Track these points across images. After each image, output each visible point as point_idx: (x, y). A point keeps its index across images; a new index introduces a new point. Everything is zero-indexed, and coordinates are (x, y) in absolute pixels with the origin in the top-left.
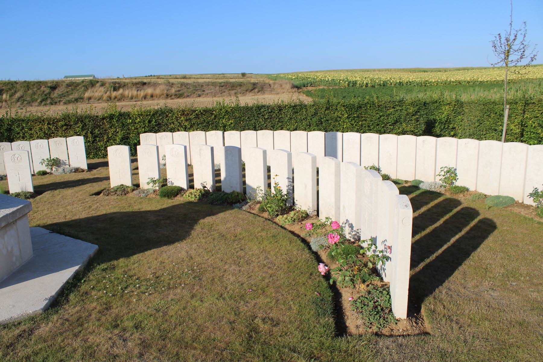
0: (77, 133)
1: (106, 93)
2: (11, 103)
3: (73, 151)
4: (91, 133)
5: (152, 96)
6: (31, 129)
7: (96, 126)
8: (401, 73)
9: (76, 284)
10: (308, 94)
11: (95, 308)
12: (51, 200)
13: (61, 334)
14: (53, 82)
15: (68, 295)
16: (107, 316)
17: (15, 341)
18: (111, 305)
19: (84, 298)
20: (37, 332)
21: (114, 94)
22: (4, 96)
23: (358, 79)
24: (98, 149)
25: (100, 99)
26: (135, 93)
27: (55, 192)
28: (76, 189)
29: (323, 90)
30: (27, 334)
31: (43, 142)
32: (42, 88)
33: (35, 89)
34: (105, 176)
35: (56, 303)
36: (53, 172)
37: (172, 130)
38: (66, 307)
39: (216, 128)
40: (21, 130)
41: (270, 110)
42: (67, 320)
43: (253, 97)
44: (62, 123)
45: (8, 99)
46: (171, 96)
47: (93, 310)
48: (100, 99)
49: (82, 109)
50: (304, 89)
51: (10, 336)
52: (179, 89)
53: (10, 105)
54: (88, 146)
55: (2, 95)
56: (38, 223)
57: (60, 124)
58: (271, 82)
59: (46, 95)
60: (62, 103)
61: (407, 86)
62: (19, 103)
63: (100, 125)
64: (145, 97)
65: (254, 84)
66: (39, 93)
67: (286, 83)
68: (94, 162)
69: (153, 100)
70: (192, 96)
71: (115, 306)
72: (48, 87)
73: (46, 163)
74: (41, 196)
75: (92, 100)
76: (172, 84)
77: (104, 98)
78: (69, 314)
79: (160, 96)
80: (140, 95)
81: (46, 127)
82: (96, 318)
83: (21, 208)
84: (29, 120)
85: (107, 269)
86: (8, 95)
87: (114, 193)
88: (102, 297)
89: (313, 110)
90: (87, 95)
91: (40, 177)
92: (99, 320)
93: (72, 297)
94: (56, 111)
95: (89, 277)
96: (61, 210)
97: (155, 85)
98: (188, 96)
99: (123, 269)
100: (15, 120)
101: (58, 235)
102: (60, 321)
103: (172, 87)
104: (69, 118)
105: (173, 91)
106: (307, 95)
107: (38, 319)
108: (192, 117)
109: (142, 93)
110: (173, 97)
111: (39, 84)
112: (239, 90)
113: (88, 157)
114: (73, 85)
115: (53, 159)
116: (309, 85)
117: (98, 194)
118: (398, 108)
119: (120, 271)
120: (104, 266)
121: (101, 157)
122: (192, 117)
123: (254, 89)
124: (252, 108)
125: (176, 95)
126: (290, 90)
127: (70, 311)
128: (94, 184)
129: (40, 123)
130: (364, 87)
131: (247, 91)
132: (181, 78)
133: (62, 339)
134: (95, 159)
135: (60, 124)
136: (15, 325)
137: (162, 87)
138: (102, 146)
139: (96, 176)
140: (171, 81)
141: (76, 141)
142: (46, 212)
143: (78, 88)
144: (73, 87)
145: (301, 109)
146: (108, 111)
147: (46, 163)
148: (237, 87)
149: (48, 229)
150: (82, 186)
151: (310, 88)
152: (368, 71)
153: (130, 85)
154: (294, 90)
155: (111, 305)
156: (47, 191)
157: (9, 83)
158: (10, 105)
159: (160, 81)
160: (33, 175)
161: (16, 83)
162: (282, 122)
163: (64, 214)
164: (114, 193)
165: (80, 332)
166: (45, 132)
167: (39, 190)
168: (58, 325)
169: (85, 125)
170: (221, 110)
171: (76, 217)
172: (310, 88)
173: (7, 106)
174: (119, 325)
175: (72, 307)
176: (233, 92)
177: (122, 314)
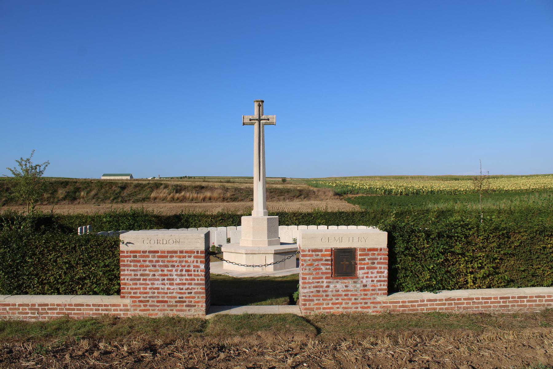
1: (170, 194)
2: (88, 200)
5: (210, 199)
6: (200, 221)
8: (433, 182)
10: (349, 201)
21: (177, 195)
22: (82, 194)
23: (394, 187)
33: (107, 189)
37: (288, 225)
44: (220, 218)
46: (227, 199)
48: (164, 199)
50: (345, 195)
60: (131, 202)
61: (434, 195)
62: (94, 200)
64: (204, 200)
65: (300, 191)
67: (329, 191)
69: (211, 202)
70: (246, 200)
72: (119, 187)
75: (157, 200)
76: (227, 189)
77: (168, 199)
79: (217, 199)
81: (209, 220)
89: (373, 215)
90: (153, 195)
97: (212, 189)
98: (242, 200)
105: (228, 194)
106: (348, 202)
108: (300, 217)
109: (201, 196)
112: (287, 196)
116: (349, 193)
118: (426, 214)
122: (300, 217)
123: (300, 195)
124: (336, 213)
125: (231, 199)
126: (333, 197)
130: (399, 195)
137: (220, 191)
140: (227, 185)
145: (366, 214)
151: (350, 196)
153: (190, 188)
157: (85, 182)
159: (217, 185)
169: (234, 220)
172: (350, 196)
176: (282, 197)
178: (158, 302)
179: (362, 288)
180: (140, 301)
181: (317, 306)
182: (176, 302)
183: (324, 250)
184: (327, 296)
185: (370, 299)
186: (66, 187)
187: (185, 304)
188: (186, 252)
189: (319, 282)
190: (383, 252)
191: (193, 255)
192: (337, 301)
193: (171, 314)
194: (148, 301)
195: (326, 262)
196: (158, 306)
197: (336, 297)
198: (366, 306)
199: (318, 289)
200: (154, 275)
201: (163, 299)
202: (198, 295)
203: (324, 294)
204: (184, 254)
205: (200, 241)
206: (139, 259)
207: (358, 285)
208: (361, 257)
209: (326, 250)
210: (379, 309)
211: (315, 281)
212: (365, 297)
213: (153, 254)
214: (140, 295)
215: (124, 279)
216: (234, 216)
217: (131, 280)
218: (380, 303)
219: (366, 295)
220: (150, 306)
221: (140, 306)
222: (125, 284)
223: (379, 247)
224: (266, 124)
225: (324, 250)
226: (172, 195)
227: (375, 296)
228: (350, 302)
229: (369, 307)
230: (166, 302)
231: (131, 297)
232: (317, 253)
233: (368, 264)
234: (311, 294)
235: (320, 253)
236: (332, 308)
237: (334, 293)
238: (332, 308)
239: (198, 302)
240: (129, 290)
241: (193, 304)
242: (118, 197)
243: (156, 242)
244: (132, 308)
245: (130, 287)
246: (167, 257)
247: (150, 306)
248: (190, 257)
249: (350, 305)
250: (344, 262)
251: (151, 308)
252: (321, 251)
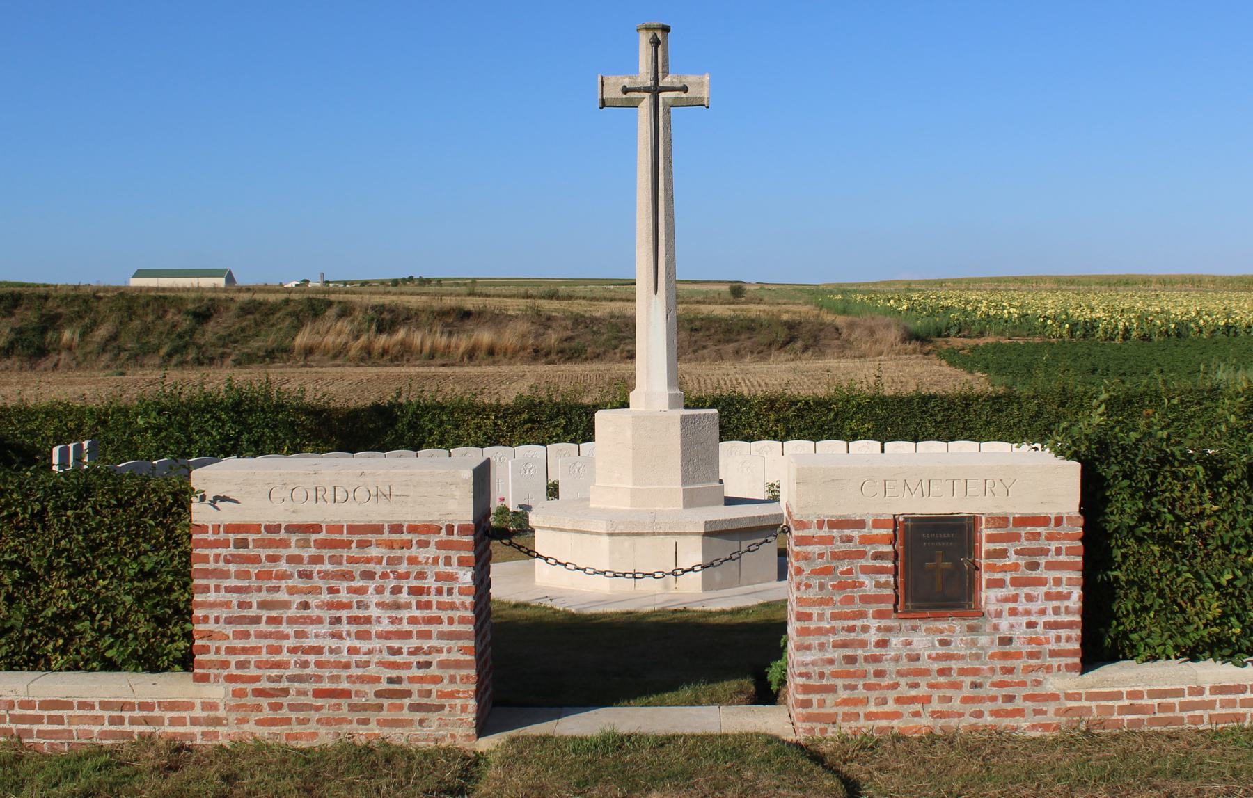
1: (357, 337)
2: (85, 355)
5: (491, 352)
6: (457, 427)
10: (954, 358)
14: (201, 300)
21: (382, 340)
22: (67, 335)
23: (1101, 315)
26: (442, 341)
29: (997, 348)
32: (169, 316)
33: (150, 318)
37: (749, 439)
39: (838, 437)
41: (946, 405)
43: (792, 364)
44: (525, 416)
46: (547, 355)
48: (338, 354)
50: (940, 342)
52: (570, 333)
53: (80, 359)
58: (840, 320)
59: (180, 336)
60: (228, 361)
62: (105, 358)
64: (471, 355)
65: (791, 326)
66: (161, 329)
67: (888, 326)
69: (494, 363)
70: (610, 355)
72: (188, 313)
75: (317, 356)
76: (549, 318)
77: (353, 352)
79: (515, 352)
80: (457, 347)
81: (489, 423)
86: (78, 332)
89: (1032, 407)
90: (301, 339)
97: (498, 319)
103: (547, 327)
105: (553, 338)
106: (951, 364)
108: (791, 413)
109: (462, 343)
110: (553, 356)
112: (748, 343)
116: (953, 331)
123: (791, 340)
124: (911, 399)
125: (562, 351)
126: (900, 346)
130: (1118, 340)
131: (770, 345)
132: (542, 297)
137: (523, 326)
140: (548, 306)
143: (273, 319)
144: (257, 316)
145: (1010, 403)
148: (739, 333)
151: (957, 342)
152: (1127, 283)
153: (423, 317)
154: (910, 347)
157: (77, 297)
159: (514, 306)
162: (971, 429)
170: (848, 401)
172: (957, 342)
173: (74, 364)
176: (730, 347)
178: (318, 693)
179: (997, 648)
180: (259, 693)
181: (846, 709)
182: (378, 694)
183: (869, 523)
184: (880, 674)
185: (1023, 684)
186: (11, 314)
187: (407, 701)
188: (413, 529)
189: (852, 629)
190: (1065, 529)
191: (434, 539)
192: (913, 693)
193: (362, 734)
194: (285, 692)
195: (877, 563)
196: (318, 709)
197: (911, 679)
198: (1009, 706)
199: (850, 652)
200: (306, 605)
201: (334, 686)
202: (452, 672)
203: (871, 668)
204: (405, 537)
205: (457, 493)
206: (257, 551)
207: (983, 640)
208: (992, 547)
209: (877, 524)
210: (1051, 718)
211: (839, 624)
212: (1008, 678)
213: (300, 536)
214: (257, 672)
215: (206, 619)
216: (571, 408)
217: (229, 621)
218: (1055, 697)
219: (1010, 671)
220: (293, 707)
221: (258, 708)
222: (209, 635)
223: (1051, 511)
224: (677, 104)
225: (869, 523)
227: (1040, 675)
228: (958, 696)
229: (1019, 712)
230: (345, 694)
231: (231, 679)
232: (847, 532)
233: (1015, 567)
234: (827, 670)
235: (856, 533)
236: (896, 715)
237: (905, 665)
238: (896, 715)
239: (451, 695)
240: (223, 656)
241: (433, 700)
242: (186, 346)
243: (312, 494)
244: (233, 716)
245: (224, 644)
246: (346, 545)
247: (293, 707)
248: (424, 544)
249: (956, 704)
250: (935, 563)
251: (294, 715)
252: (860, 524)
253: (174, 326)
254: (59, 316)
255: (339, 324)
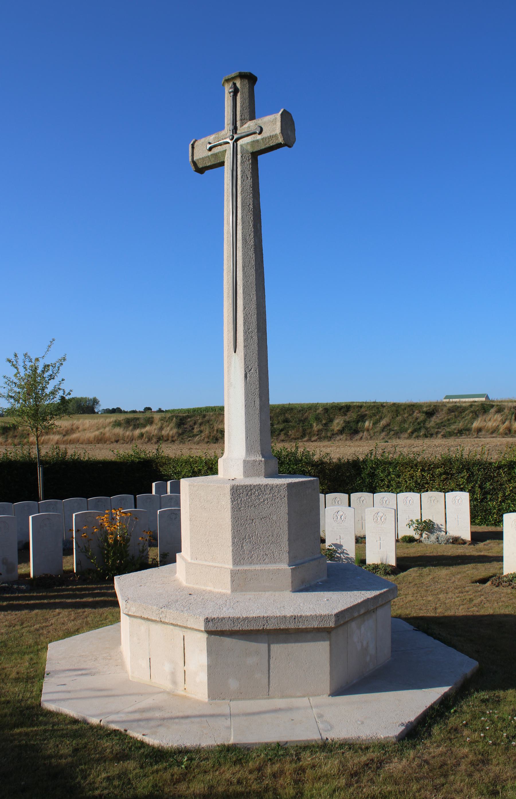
0: (459, 485)
1: (504, 423)
2: (374, 433)
3: (453, 512)
4: (480, 487)
6: (399, 476)
7: (487, 478)
9: (443, 713)
11: (467, 757)
12: (417, 581)
13: (418, 780)
14: (430, 406)
15: (430, 726)
16: (482, 773)
17: (361, 770)
18: (490, 757)
19: (453, 737)
20: (387, 767)
22: (367, 424)
24: (488, 512)
25: (494, 431)
27: (424, 570)
28: (453, 569)
30: (375, 765)
31: (414, 496)
32: (415, 414)
33: (406, 415)
34: (495, 555)
35: (415, 732)
36: (422, 539)
38: (427, 742)
40: (387, 476)
42: (427, 762)
45: (370, 428)
47: (463, 758)
48: (494, 431)
49: (468, 447)
51: (356, 761)
54: (474, 506)
55: (365, 422)
56: (399, 612)
57: (438, 471)
59: (419, 424)
60: (439, 436)
62: (383, 434)
63: (494, 477)
66: (410, 420)
68: (480, 530)
71: (495, 761)
72: (423, 412)
73: (414, 525)
74: (405, 573)
75: (483, 433)
77: (501, 430)
78: (430, 753)
81: (418, 474)
82: (466, 770)
83: (384, 592)
84: (398, 463)
85: (488, 700)
86: (372, 422)
87: (507, 584)
88: (478, 741)
90: (476, 424)
91: (405, 544)
92: (470, 775)
93: (436, 730)
94: (434, 448)
95: (461, 707)
96: (430, 598)
99: (512, 707)
100: (380, 462)
101: (425, 636)
102: (417, 761)
104: (451, 464)
107: (390, 749)
111: (412, 407)
113: (473, 522)
114: (457, 411)
115: (425, 522)
117: (483, 581)
119: (507, 708)
120: (484, 695)
121: (492, 524)
127: (431, 750)
128: (479, 565)
129: (412, 468)
133: (418, 787)
134: (482, 526)
135: (438, 471)
136: (361, 749)
138: (495, 508)
139: (482, 554)
141: (458, 498)
142: (410, 598)
143: (464, 415)
144: (456, 413)
146: (506, 456)
147: (414, 525)
149: (411, 624)
150: (461, 566)
155: (490, 757)
156: (414, 567)
157: (374, 406)
158: (372, 435)
160: (397, 541)
161: (382, 405)
163: (434, 605)
164: (507, 584)
165: (443, 785)
166: (416, 481)
167: (403, 564)
168: (414, 765)
169: (472, 475)
171: (450, 613)
174: (498, 793)
175: (435, 745)
177: (504, 777)
226: (507, 423)
253: (417, 419)
254: (365, 415)
255: (496, 416)
